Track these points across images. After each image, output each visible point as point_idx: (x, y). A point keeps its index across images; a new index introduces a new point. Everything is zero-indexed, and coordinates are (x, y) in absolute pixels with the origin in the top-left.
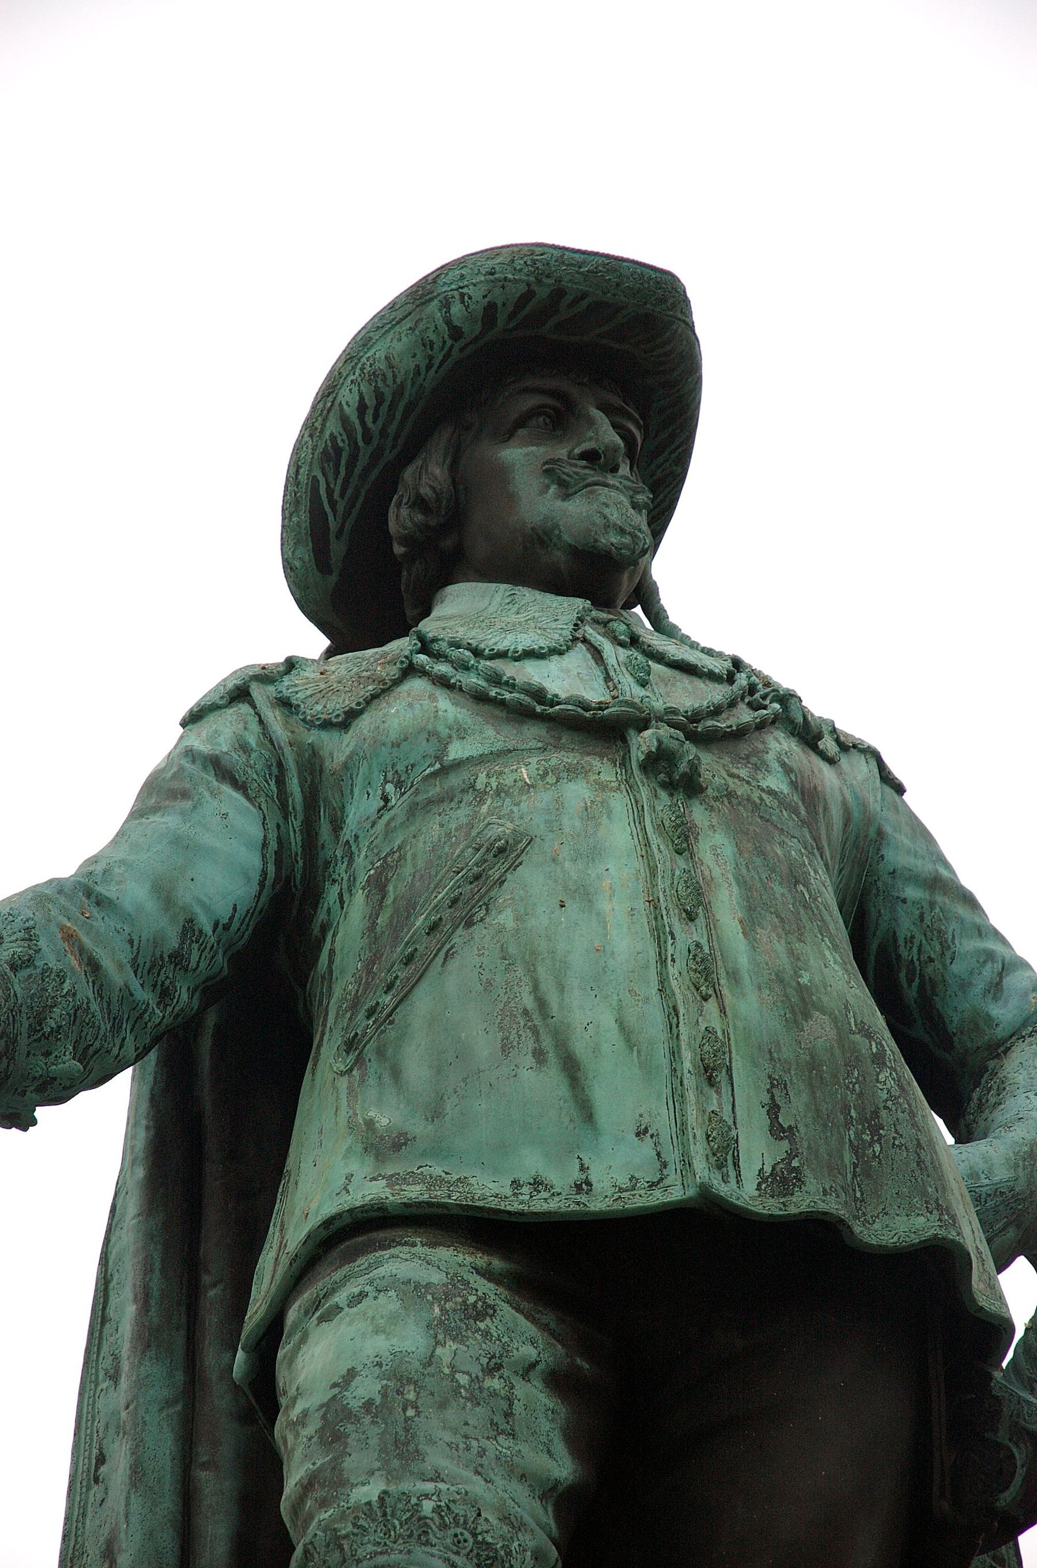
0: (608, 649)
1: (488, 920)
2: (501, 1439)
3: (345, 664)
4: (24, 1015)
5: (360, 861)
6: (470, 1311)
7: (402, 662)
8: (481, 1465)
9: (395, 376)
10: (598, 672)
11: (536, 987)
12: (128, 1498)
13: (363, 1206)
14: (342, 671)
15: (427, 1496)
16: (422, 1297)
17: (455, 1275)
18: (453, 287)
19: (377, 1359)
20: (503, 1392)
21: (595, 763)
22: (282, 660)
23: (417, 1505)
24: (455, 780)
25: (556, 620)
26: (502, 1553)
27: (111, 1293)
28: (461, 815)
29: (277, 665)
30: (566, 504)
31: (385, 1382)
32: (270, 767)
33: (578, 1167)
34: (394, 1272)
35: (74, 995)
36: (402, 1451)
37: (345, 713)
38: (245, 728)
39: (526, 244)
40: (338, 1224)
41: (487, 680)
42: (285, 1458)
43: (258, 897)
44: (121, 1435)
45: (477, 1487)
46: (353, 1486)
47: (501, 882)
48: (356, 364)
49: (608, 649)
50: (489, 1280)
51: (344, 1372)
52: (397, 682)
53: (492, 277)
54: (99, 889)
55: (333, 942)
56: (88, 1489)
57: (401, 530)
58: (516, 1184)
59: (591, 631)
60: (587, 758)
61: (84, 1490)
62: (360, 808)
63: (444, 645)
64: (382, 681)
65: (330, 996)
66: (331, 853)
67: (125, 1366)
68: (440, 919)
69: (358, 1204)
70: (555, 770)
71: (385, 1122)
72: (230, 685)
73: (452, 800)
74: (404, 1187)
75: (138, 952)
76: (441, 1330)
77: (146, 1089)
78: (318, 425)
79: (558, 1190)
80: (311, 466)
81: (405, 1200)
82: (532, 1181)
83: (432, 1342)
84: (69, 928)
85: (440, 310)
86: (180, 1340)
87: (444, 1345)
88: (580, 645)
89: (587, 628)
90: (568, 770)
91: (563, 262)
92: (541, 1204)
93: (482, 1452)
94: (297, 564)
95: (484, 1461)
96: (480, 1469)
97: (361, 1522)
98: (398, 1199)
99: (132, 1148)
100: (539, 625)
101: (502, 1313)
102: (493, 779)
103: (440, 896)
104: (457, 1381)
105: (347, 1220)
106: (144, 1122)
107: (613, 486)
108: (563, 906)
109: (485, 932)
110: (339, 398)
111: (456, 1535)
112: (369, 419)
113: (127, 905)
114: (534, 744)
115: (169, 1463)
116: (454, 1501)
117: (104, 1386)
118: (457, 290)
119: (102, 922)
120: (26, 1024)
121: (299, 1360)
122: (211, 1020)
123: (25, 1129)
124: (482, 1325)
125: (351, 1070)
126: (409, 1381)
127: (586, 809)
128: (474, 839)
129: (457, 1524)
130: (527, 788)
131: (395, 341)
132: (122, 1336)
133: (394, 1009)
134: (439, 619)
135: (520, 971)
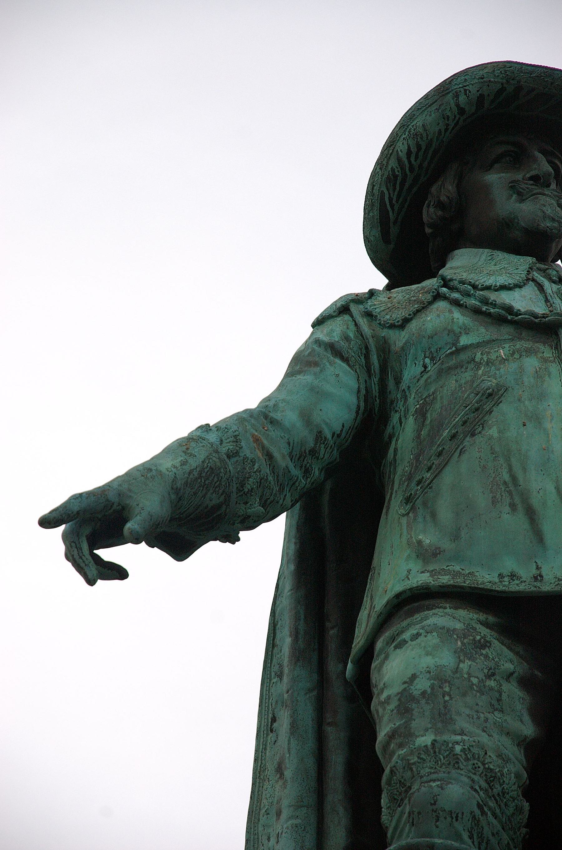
0: (547, 285)
1: (483, 433)
2: (496, 713)
3: (399, 293)
4: (235, 483)
5: (411, 400)
6: (477, 644)
7: (433, 292)
8: (486, 727)
9: (427, 135)
10: (541, 297)
11: (510, 470)
12: (289, 741)
13: (417, 587)
14: (400, 297)
15: (457, 743)
16: (451, 636)
17: (469, 624)
18: (461, 86)
19: (428, 669)
20: (496, 688)
21: (541, 347)
22: (367, 291)
23: (452, 747)
24: (463, 356)
25: (517, 269)
26: (499, 774)
27: (277, 631)
28: (467, 376)
29: (364, 294)
30: (522, 205)
31: (432, 681)
32: (361, 349)
33: (535, 567)
34: (435, 622)
35: (260, 471)
36: (443, 719)
37: (402, 320)
38: (348, 328)
39: (502, 62)
40: (403, 596)
41: (481, 302)
42: (377, 721)
43: (355, 420)
44: (284, 707)
45: (484, 738)
46: (417, 737)
47: (490, 412)
48: (406, 129)
49: (547, 285)
50: (487, 627)
51: (410, 675)
52: (431, 303)
53: (482, 80)
54: (271, 414)
55: (396, 444)
56: (267, 735)
57: (429, 219)
58: (501, 576)
59: (537, 275)
60: (536, 345)
61: (265, 735)
62: (411, 371)
63: (456, 283)
64: (423, 303)
65: (395, 474)
66: (394, 396)
67: (286, 670)
68: (457, 432)
69: (414, 585)
70: (519, 351)
71: (428, 541)
72: (339, 305)
73: (462, 367)
74: (439, 577)
75: (293, 449)
76: (462, 654)
77: (294, 523)
78: (384, 162)
79: (524, 579)
80: (380, 185)
81: (441, 584)
82: (510, 574)
83: (458, 660)
84: (256, 436)
85: (453, 99)
86: (315, 657)
87: (464, 662)
88: (530, 282)
89: (534, 273)
90: (526, 351)
91: (522, 72)
92: (515, 587)
93: (486, 720)
94: (372, 239)
95: (488, 725)
96: (485, 729)
97: (422, 756)
98: (437, 583)
99: (287, 554)
100: (508, 271)
101: (494, 645)
102: (485, 356)
103: (457, 419)
104: (472, 682)
105: (409, 594)
106: (293, 540)
107: (547, 195)
108: (524, 425)
109: (482, 439)
110: (397, 148)
111: (474, 764)
112: (413, 159)
113: (287, 424)
114: (507, 337)
115: (311, 722)
116: (472, 746)
117: (275, 680)
118: (462, 87)
119: (274, 433)
120: (235, 486)
121: (384, 669)
122: (328, 486)
123: (234, 543)
124: (484, 652)
125: (408, 513)
126: (446, 681)
127: (537, 372)
128: (475, 389)
129: (474, 759)
130: (503, 361)
131: (428, 116)
132: (284, 654)
133: (432, 480)
134: (451, 268)
135: (502, 461)
